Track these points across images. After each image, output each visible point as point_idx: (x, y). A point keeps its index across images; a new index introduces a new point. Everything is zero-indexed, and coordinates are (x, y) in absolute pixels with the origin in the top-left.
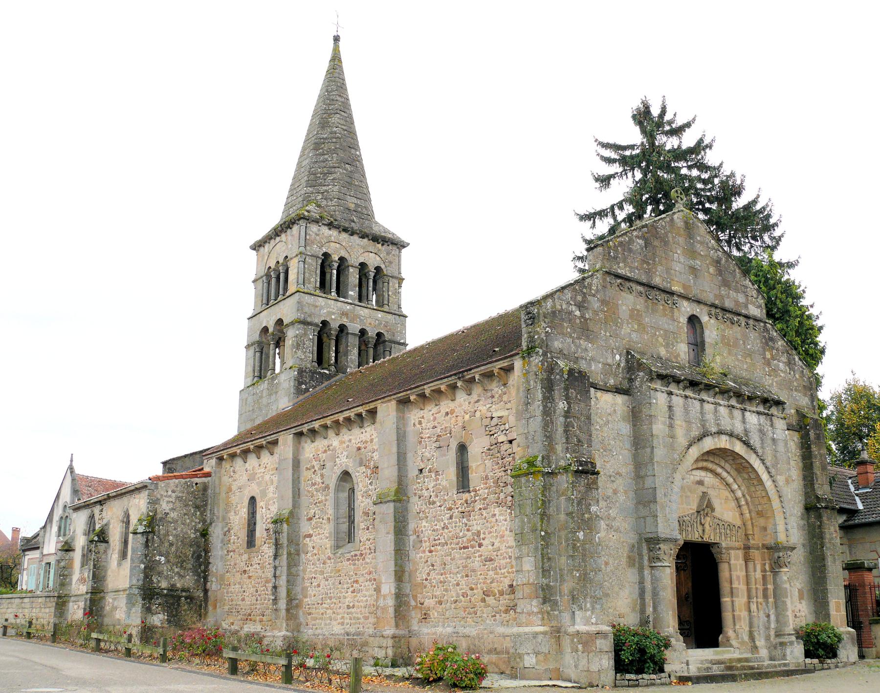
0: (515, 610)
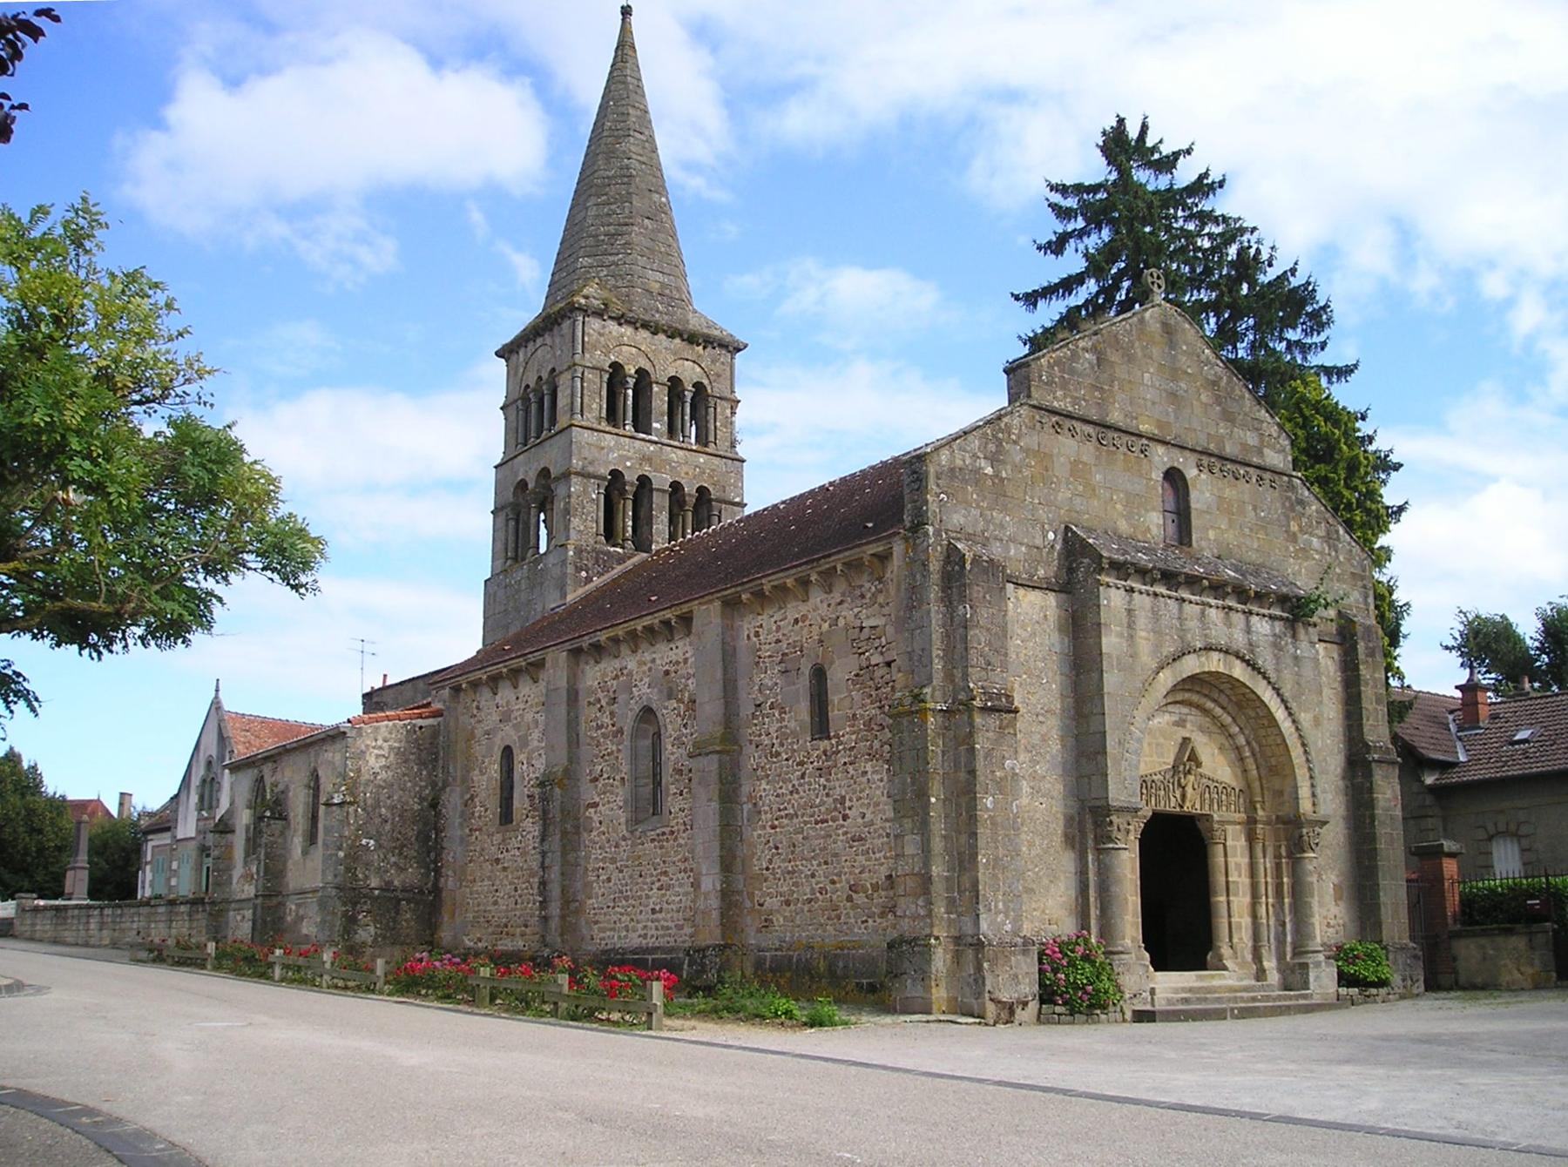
0: (895, 913)
